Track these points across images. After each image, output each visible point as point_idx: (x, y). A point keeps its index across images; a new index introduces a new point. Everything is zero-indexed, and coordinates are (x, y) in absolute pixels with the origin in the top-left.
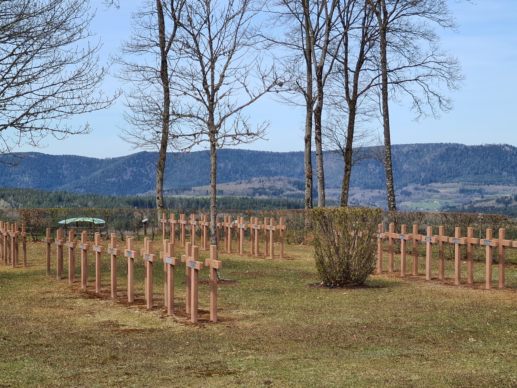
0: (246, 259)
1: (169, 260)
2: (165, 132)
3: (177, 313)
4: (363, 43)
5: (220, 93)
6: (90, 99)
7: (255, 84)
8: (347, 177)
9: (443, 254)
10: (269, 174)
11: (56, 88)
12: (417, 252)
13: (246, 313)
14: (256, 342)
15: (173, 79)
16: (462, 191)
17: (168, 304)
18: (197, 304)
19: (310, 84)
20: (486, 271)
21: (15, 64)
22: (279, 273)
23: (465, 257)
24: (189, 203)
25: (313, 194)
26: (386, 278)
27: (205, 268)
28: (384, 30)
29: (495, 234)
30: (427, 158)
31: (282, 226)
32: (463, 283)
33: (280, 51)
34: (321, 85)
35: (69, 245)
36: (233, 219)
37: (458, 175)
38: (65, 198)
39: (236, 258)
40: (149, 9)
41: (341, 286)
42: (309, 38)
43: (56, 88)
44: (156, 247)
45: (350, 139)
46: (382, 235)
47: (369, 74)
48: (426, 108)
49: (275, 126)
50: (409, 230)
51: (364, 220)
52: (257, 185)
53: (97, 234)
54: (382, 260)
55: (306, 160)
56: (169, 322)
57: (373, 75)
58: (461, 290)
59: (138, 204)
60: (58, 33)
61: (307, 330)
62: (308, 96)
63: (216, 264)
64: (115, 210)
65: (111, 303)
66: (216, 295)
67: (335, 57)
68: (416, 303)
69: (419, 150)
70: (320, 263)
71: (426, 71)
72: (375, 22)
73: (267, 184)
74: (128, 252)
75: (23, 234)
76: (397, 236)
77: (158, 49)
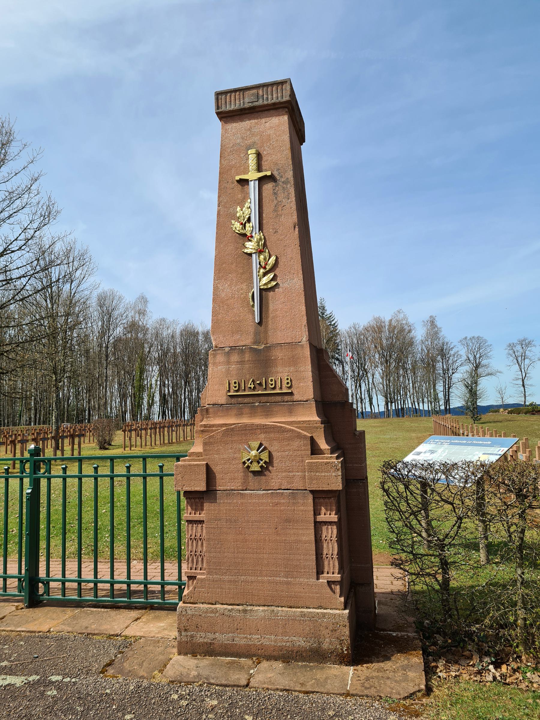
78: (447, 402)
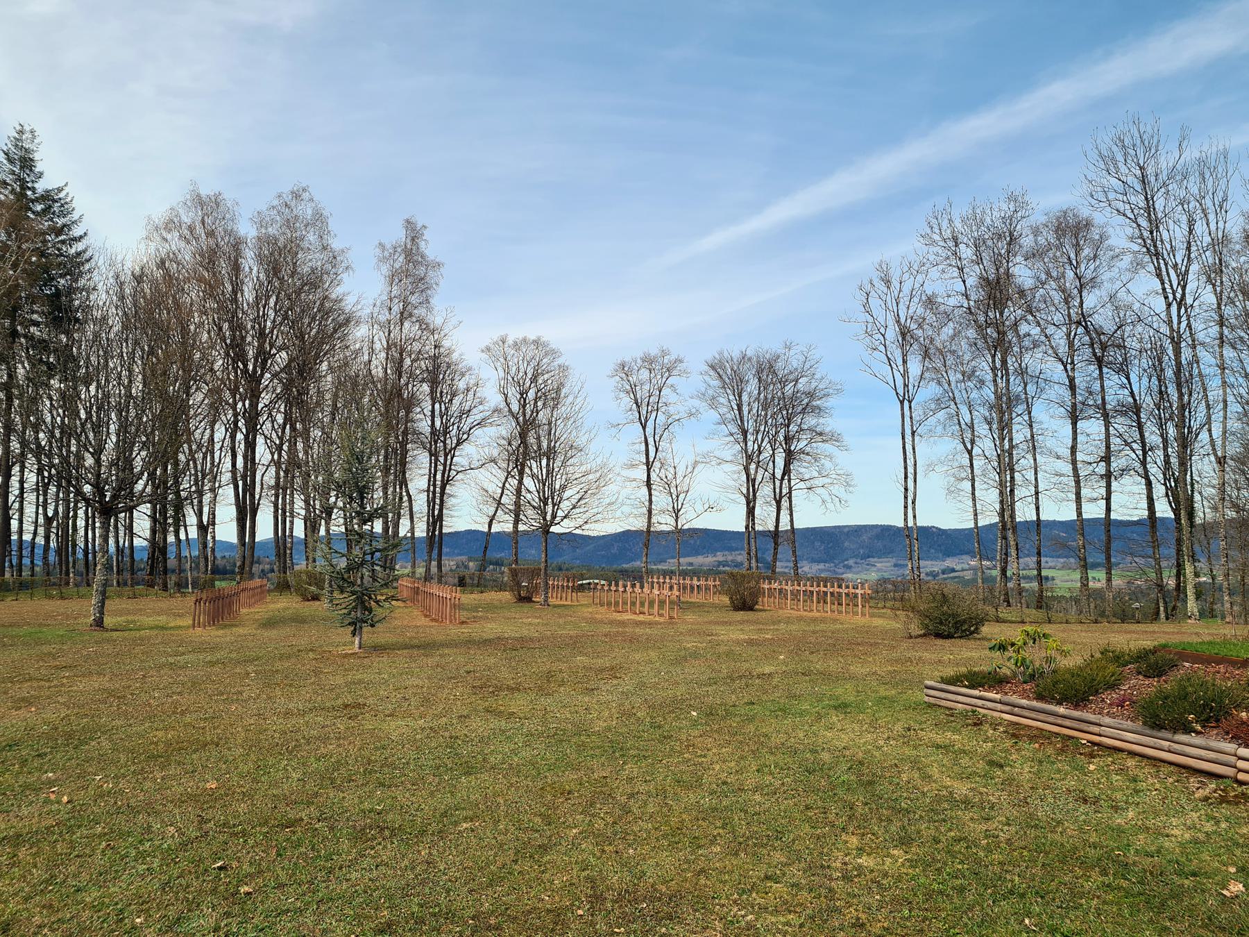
7: (699, 508)
10: (731, 549)
16: (895, 565)
37: (892, 552)
48: (830, 505)
52: (721, 559)
62: (747, 498)
71: (829, 481)
73: (730, 558)
78: (434, 523)
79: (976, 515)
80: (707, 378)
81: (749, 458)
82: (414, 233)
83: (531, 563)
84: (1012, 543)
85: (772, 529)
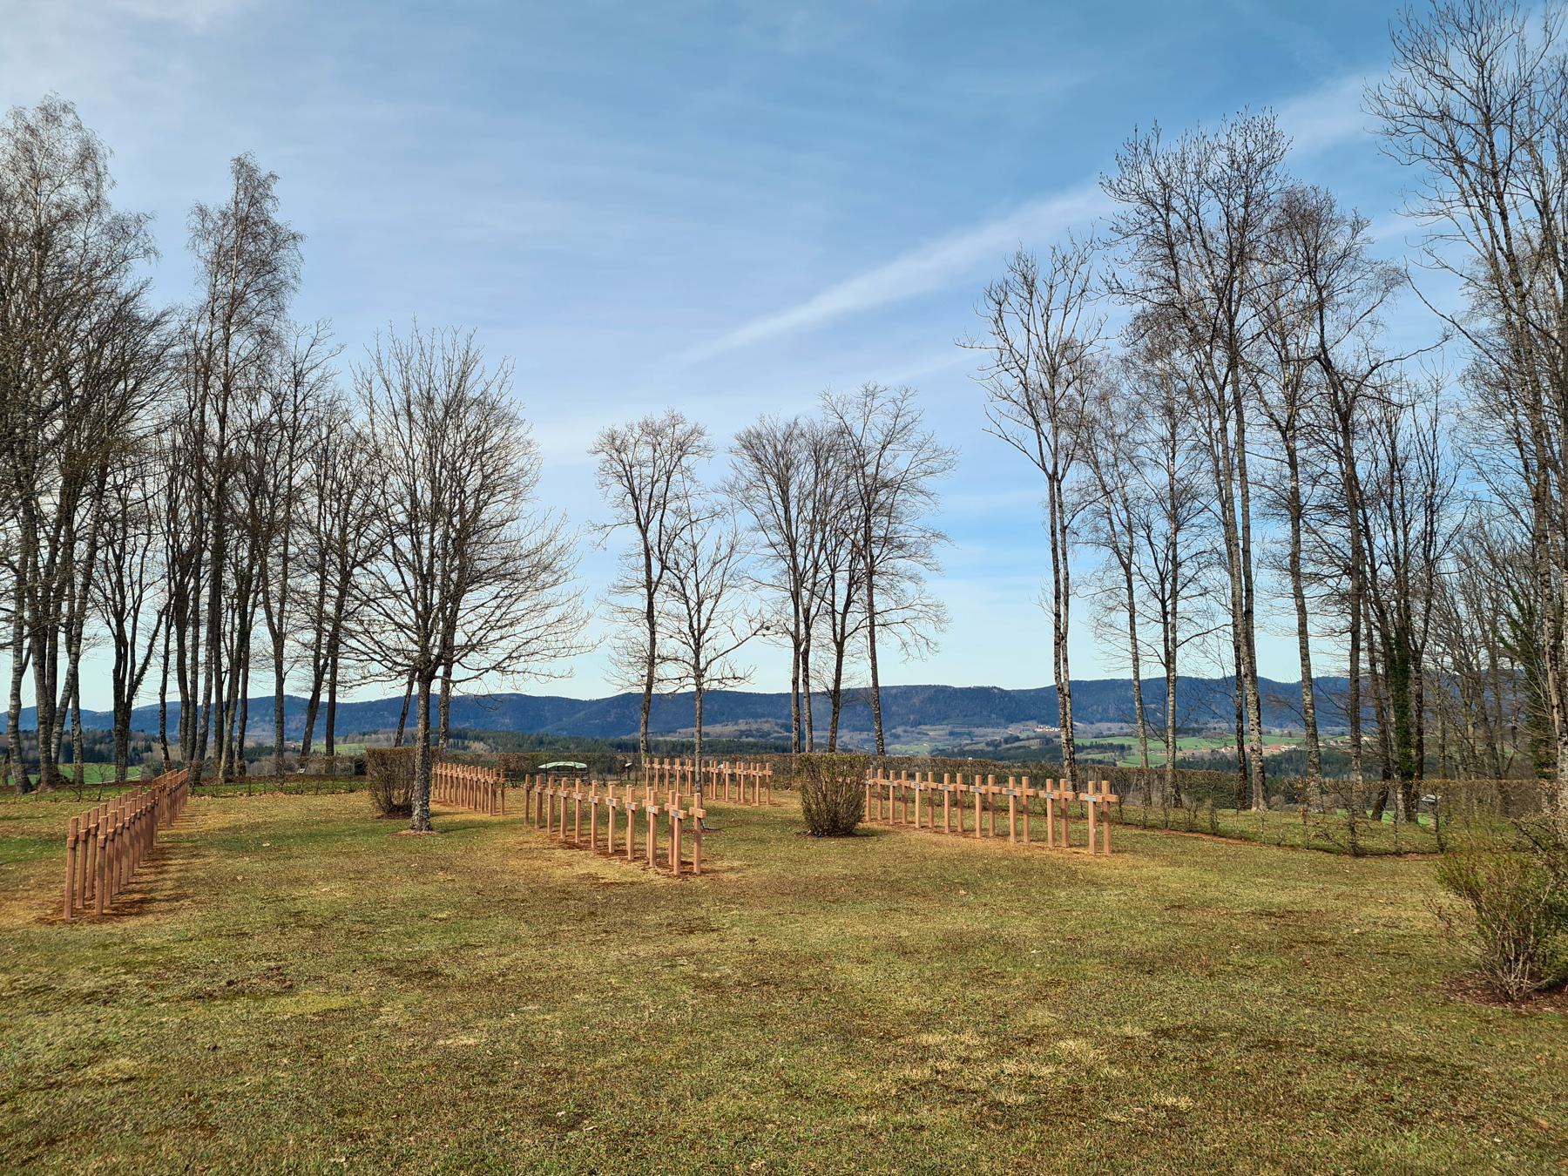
0: (732, 805)
1: (652, 809)
2: (650, 676)
3: (659, 865)
4: (850, 586)
5: (705, 637)
6: (574, 642)
7: (743, 629)
8: (835, 720)
9: (932, 802)
10: (756, 716)
11: (540, 631)
12: (906, 799)
13: (731, 864)
14: (742, 896)
15: (659, 621)
16: (951, 734)
17: (650, 855)
18: (680, 854)
19: (797, 626)
20: (976, 818)
21: (498, 607)
22: (766, 822)
23: (955, 803)
24: (674, 745)
25: (801, 736)
26: (875, 826)
27: (689, 817)
28: (871, 572)
29: (984, 782)
30: (916, 700)
31: (768, 772)
32: (953, 831)
33: (766, 592)
34: (808, 628)
35: (549, 792)
36: (719, 763)
38: (546, 740)
39: (721, 804)
40: (636, 551)
41: (829, 835)
42: (796, 580)
43: (540, 631)
44: (639, 793)
45: (838, 681)
46: (870, 782)
47: (856, 616)
48: (913, 650)
49: (764, 670)
50: (898, 776)
51: (852, 767)
52: (743, 727)
53: (578, 781)
54: (871, 806)
55: (793, 702)
56: (651, 875)
57: (860, 617)
58: (951, 839)
59: (622, 747)
60: (544, 575)
61: (794, 883)
63: (700, 813)
64: (598, 754)
65: (591, 854)
66: (700, 845)
67: (822, 599)
68: (906, 853)
69: (908, 692)
70: (808, 810)
72: (862, 565)
73: (755, 726)
74: (610, 801)
75: (502, 780)
76: (885, 782)
77: (645, 591)
79: (1136, 660)
80: (737, 459)
81: (799, 581)
82: (252, 185)
83: (426, 750)
84: (1251, 698)
85: (831, 687)
